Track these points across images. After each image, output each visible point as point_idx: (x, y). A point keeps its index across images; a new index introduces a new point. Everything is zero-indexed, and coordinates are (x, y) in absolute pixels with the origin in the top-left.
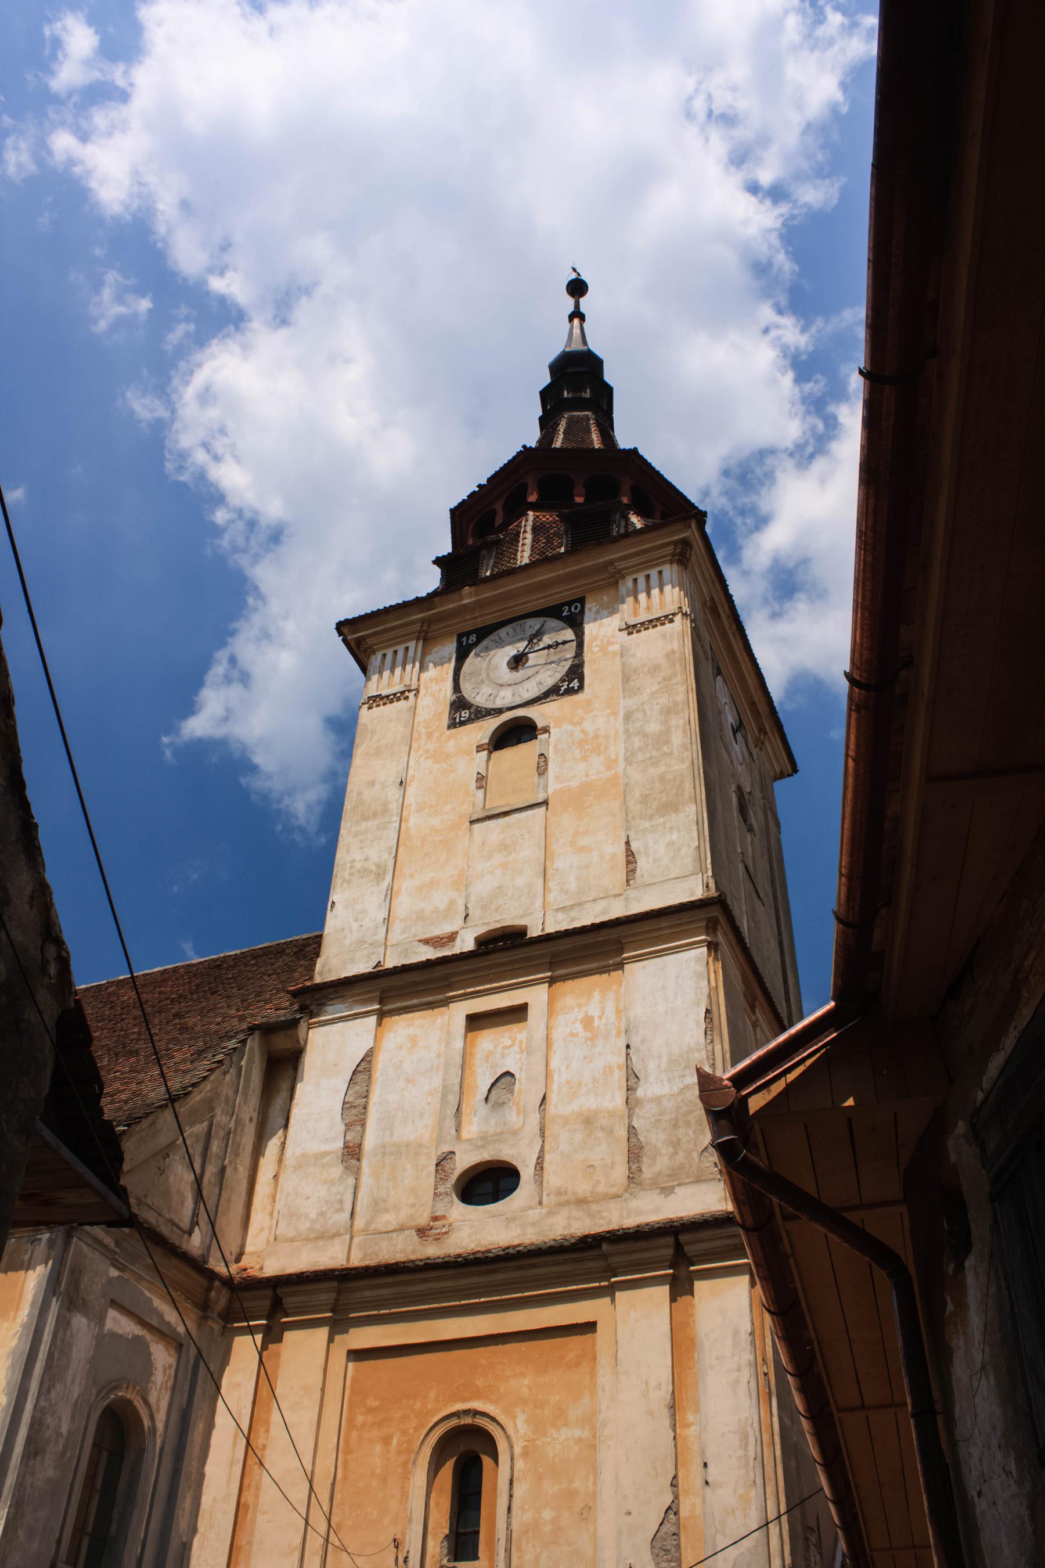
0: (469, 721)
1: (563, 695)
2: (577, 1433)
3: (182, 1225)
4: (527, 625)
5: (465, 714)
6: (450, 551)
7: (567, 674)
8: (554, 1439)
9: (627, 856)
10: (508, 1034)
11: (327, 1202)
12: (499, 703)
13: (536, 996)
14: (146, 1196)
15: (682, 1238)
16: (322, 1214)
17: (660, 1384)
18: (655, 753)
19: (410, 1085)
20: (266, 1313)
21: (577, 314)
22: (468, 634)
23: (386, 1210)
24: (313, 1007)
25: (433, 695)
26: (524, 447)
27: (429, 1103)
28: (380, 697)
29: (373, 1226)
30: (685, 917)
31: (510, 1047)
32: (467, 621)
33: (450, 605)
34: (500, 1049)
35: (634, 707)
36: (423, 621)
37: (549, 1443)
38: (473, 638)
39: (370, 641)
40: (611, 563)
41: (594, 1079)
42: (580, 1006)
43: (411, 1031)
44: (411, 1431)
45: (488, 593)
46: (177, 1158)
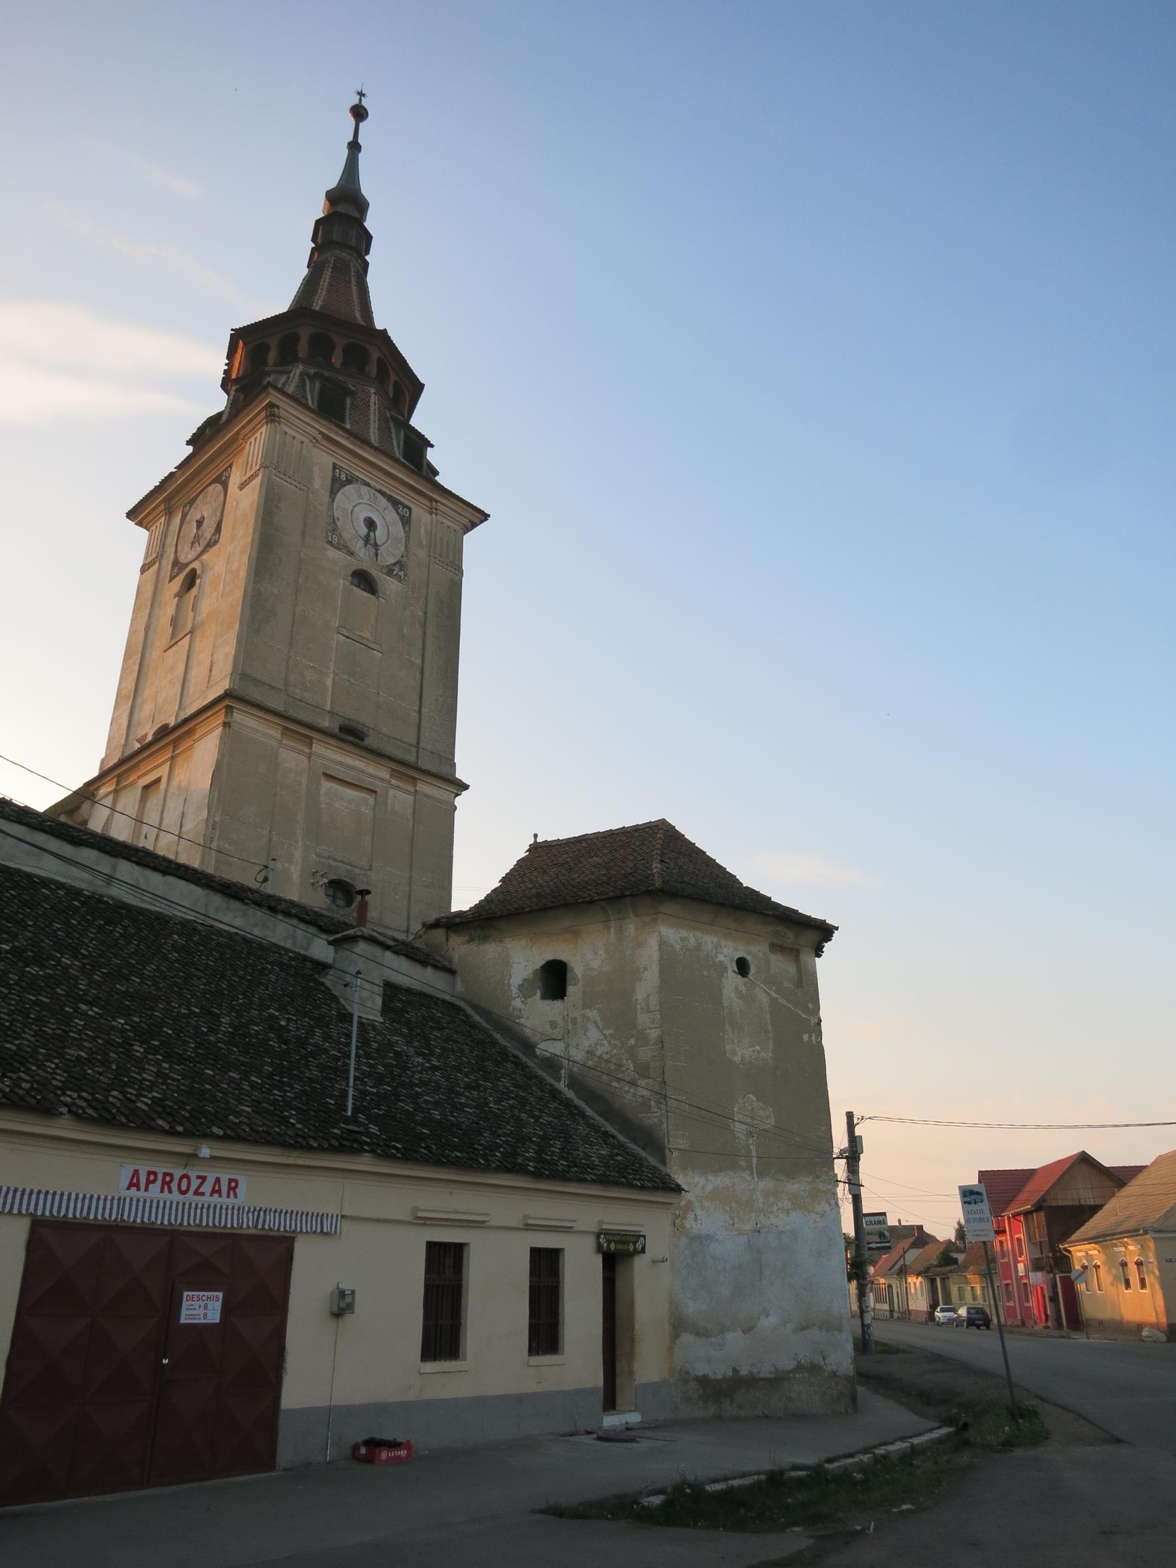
36: (163, 501)
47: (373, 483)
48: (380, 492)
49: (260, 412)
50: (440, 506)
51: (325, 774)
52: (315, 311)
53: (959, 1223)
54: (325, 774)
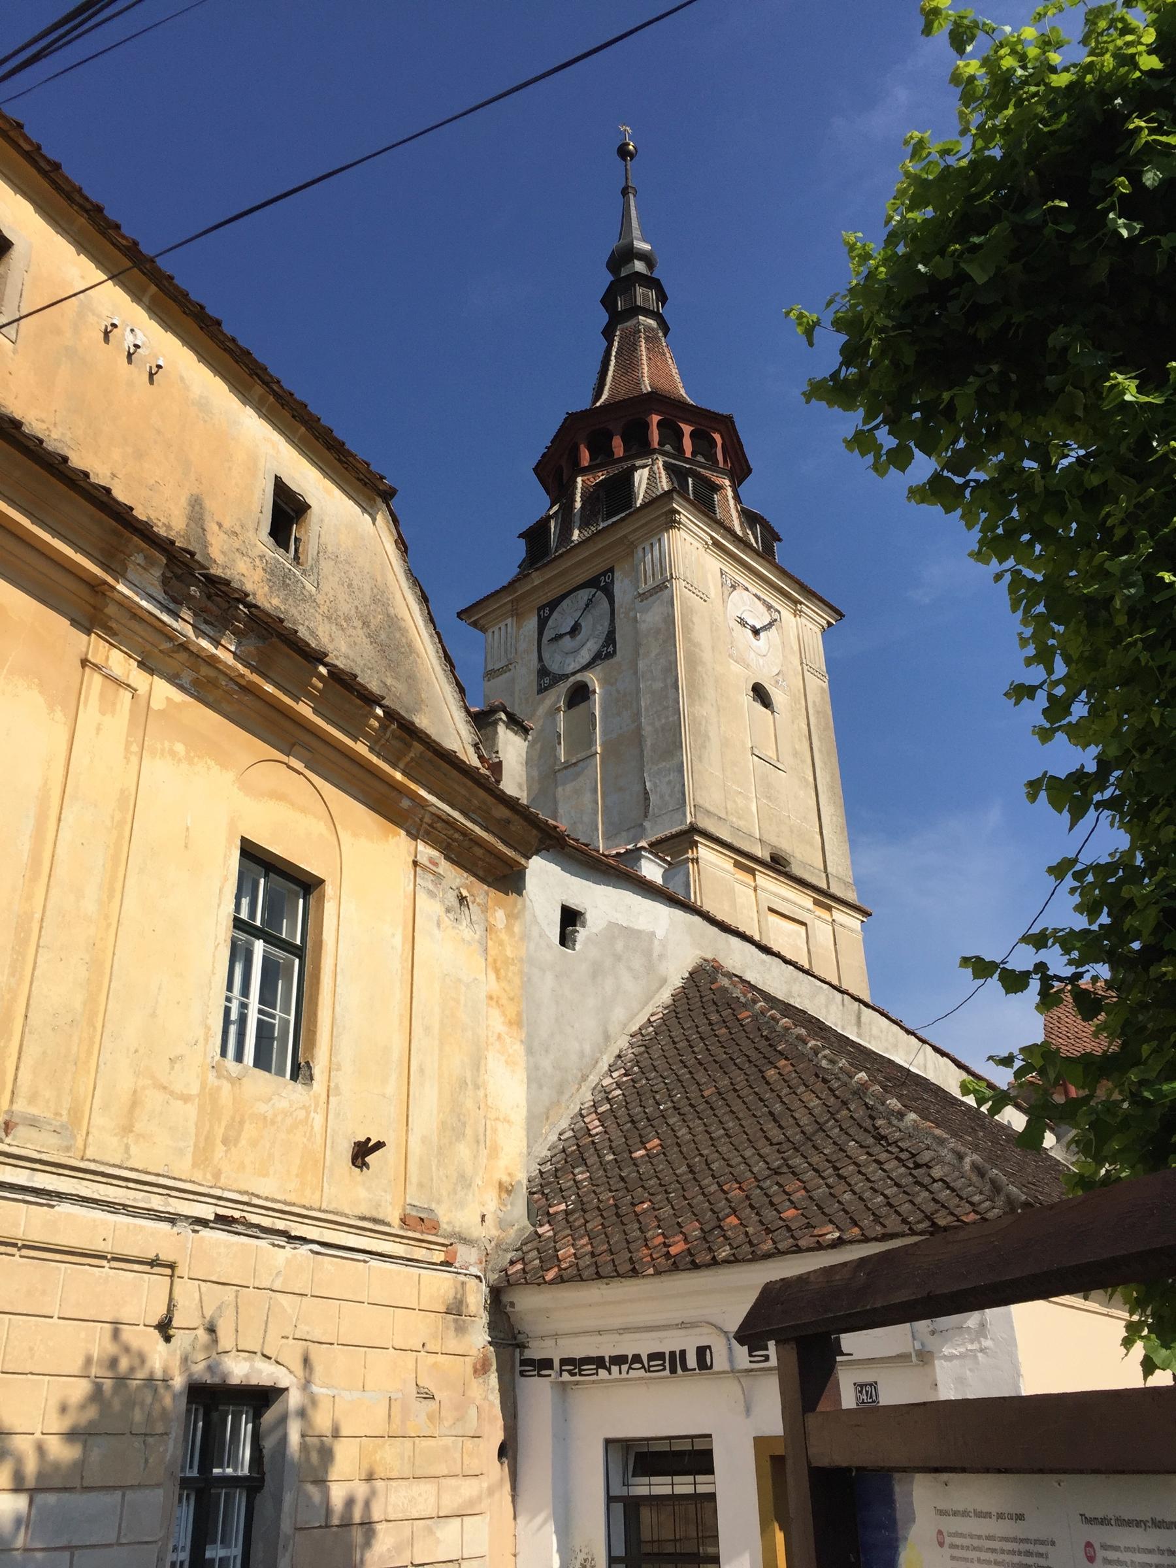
36: (512, 601)
40: (625, 536)
47: (750, 587)
48: (756, 595)
49: (659, 516)
50: (804, 608)
51: (771, 910)
52: (649, 393)
53: (369, 1140)
54: (771, 910)
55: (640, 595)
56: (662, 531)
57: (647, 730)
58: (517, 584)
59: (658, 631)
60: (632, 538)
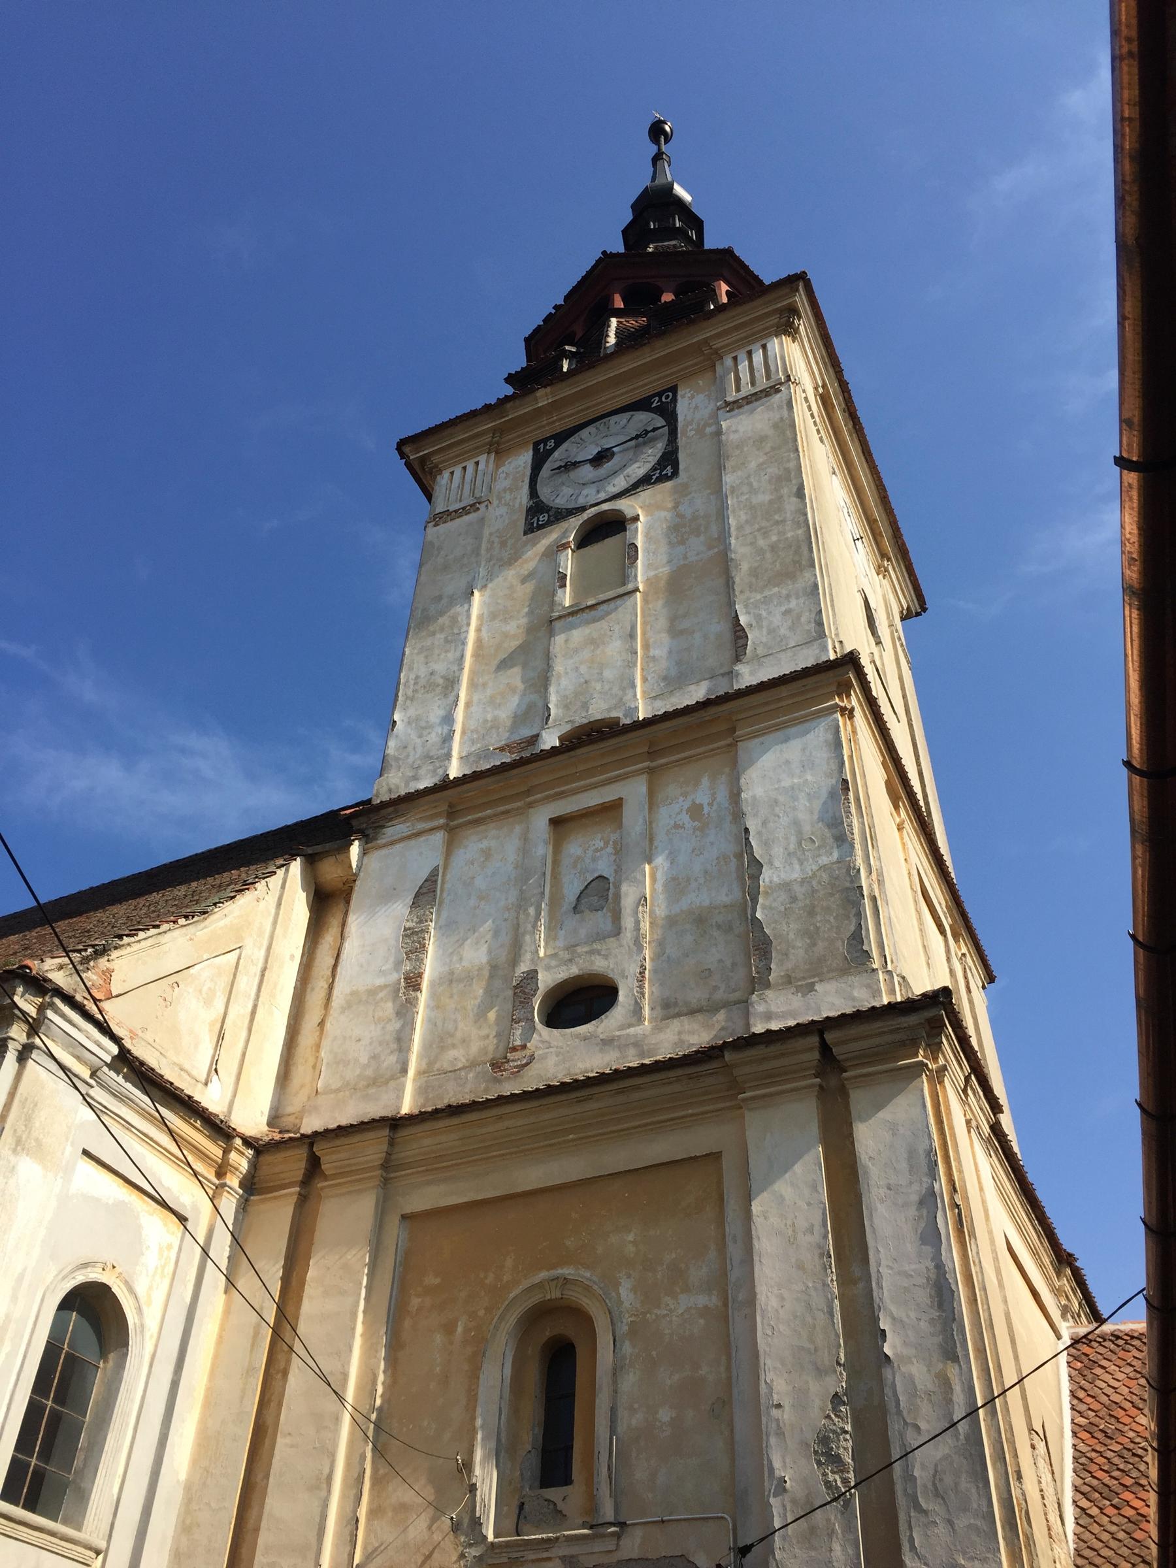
0: (549, 523)
1: (654, 483)
2: (702, 1300)
3: (195, 1073)
4: (612, 422)
5: (543, 518)
6: (524, 365)
7: (659, 462)
8: (671, 1310)
9: (736, 632)
10: (599, 836)
11: (380, 1044)
12: (581, 501)
13: (633, 791)
14: (144, 1029)
15: (829, 1037)
16: (375, 1057)
17: (813, 1225)
18: (764, 524)
19: (483, 903)
20: (300, 1178)
21: (657, 158)
22: (545, 441)
23: (454, 1046)
24: (370, 832)
25: (507, 504)
26: (604, 253)
27: (506, 920)
28: (447, 513)
29: (437, 1066)
30: (810, 681)
31: (602, 849)
32: (544, 426)
33: (524, 409)
34: (590, 853)
35: (737, 482)
36: (494, 430)
37: (665, 1316)
38: (551, 443)
39: (436, 459)
40: (706, 342)
41: (706, 872)
42: (685, 795)
43: (485, 844)
44: (481, 1313)
45: (565, 390)
46: (191, 990)
49: (768, 315)
51: (86, 1153)
54: (86, 1153)
55: (727, 404)
56: (769, 335)
57: (739, 549)
58: (509, 405)
59: (762, 439)
60: (717, 344)
